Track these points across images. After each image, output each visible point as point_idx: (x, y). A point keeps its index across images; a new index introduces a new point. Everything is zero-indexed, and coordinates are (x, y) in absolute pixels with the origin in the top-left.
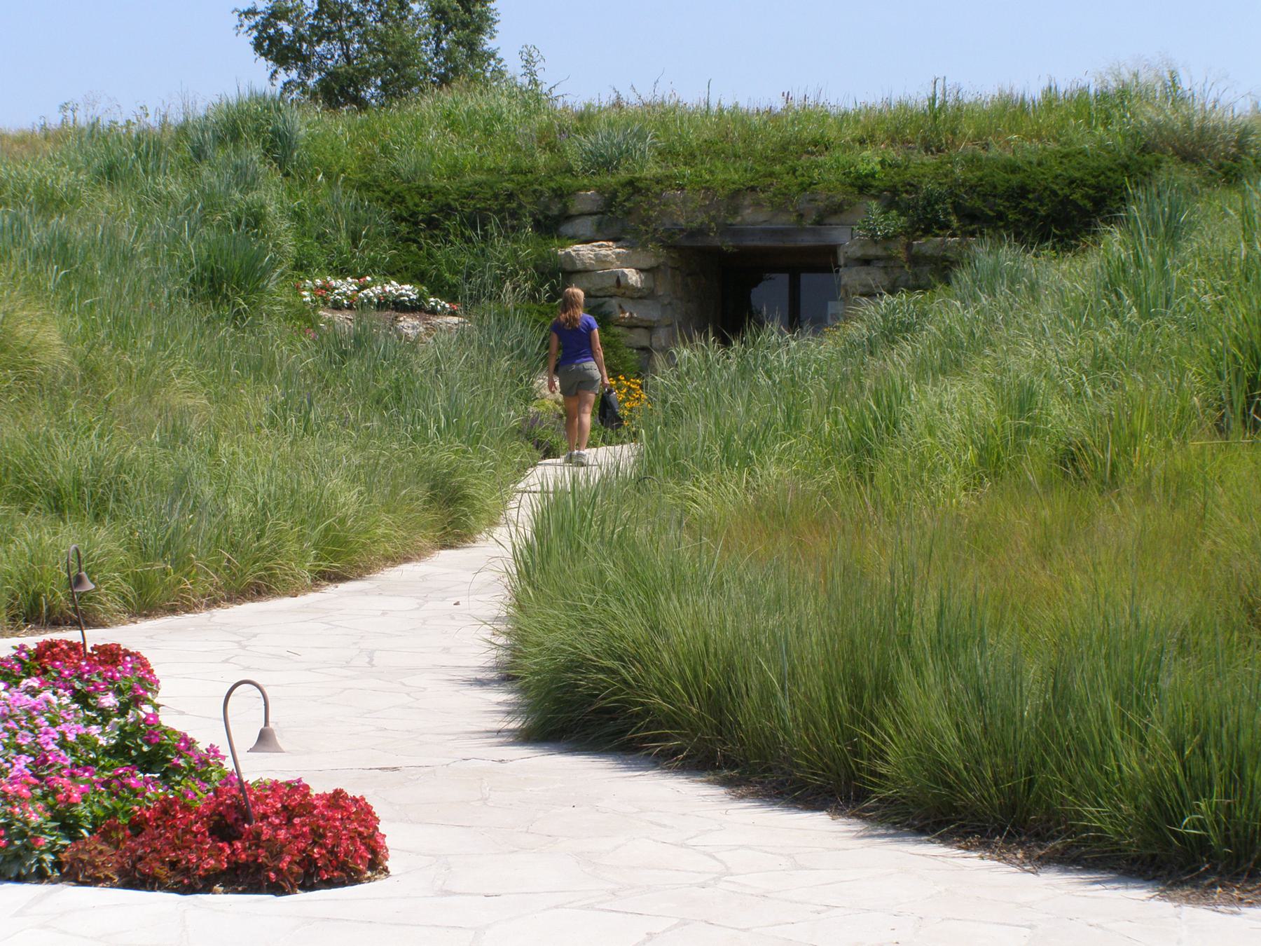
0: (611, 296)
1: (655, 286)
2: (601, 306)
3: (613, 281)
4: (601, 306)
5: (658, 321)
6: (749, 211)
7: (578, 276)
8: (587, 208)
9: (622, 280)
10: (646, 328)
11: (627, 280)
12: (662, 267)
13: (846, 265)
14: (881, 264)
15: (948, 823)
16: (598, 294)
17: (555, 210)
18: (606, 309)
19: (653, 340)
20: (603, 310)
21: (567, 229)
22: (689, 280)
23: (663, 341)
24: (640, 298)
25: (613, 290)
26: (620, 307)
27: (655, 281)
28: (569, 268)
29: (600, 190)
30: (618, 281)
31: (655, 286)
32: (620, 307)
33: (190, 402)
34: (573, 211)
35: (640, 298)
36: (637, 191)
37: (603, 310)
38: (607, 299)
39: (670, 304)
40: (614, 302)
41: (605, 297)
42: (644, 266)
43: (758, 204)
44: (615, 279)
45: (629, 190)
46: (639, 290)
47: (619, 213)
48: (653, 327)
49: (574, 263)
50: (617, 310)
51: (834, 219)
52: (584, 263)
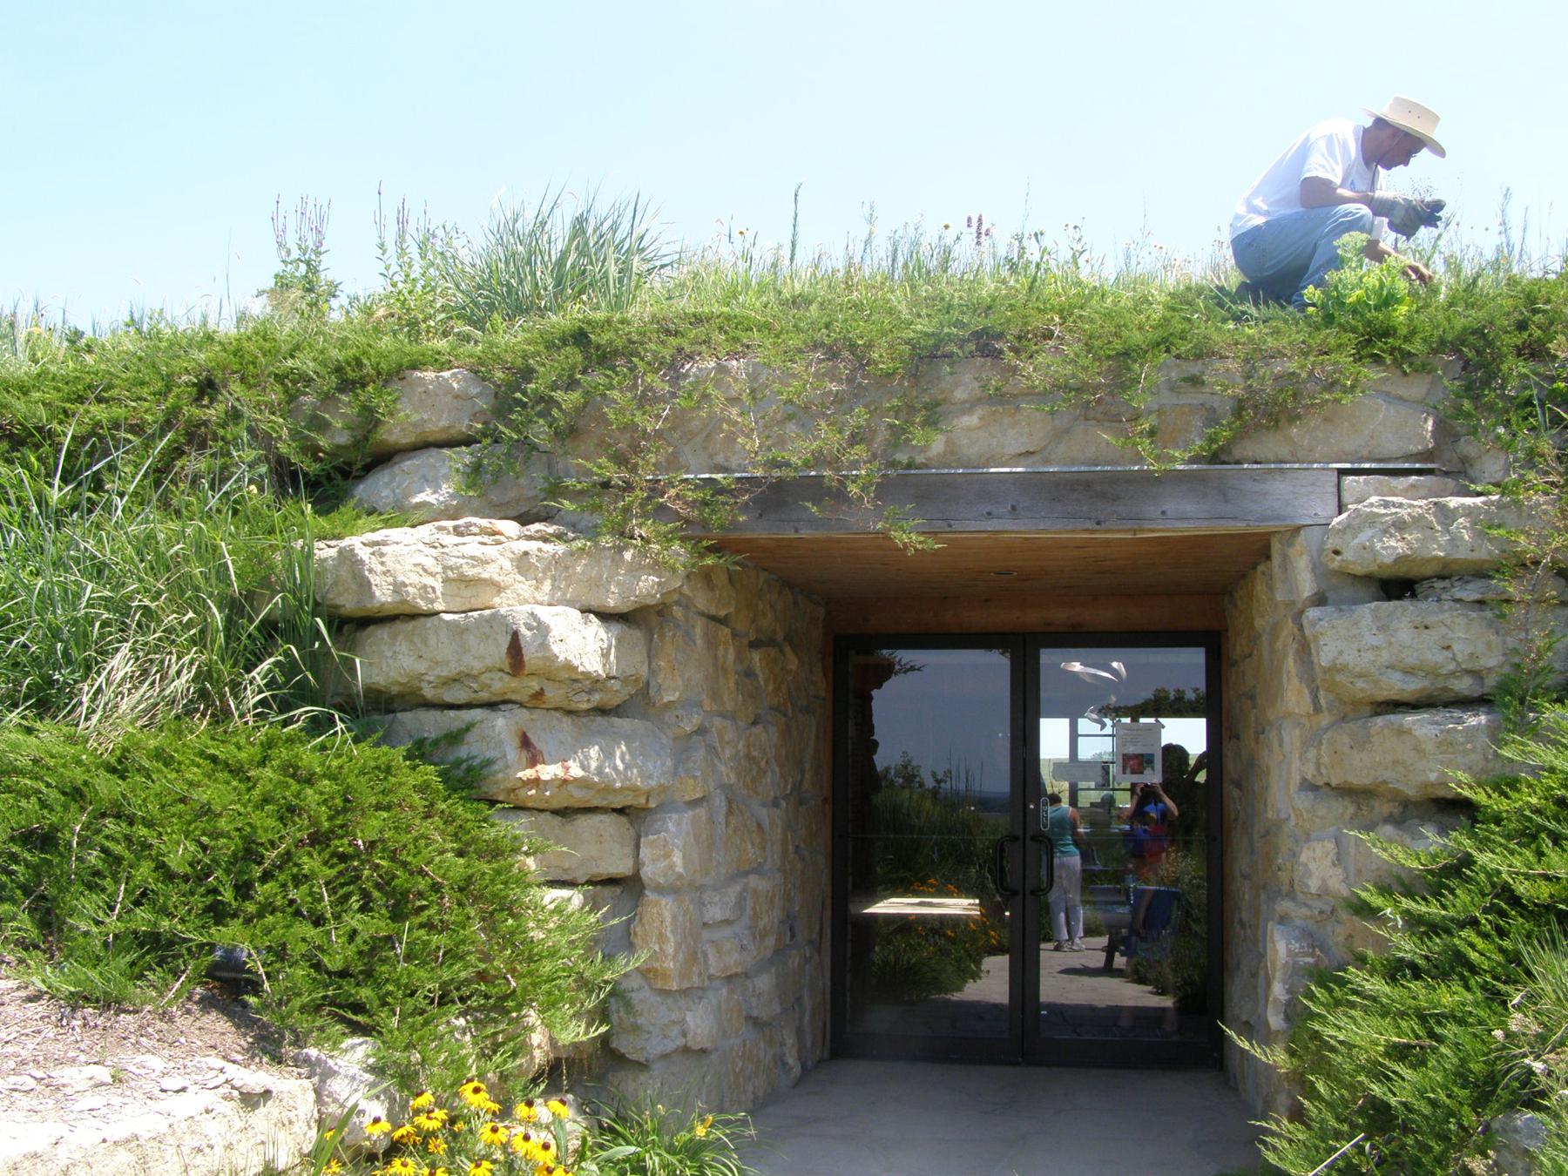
0: (491, 705)
1: (652, 672)
2: (455, 738)
3: (498, 651)
4: (455, 738)
5: (663, 789)
6: (972, 420)
7: (382, 633)
8: (439, 422)
9: (530, 653)
10: (621, 811)
11: (544, 646)
12: (678, 612)
13: (1320, 600)
14: (1471, 592)
15: (547, 518)
16: (449, 697)
17: (337, 434)
18: (472, 748)
19: (645, 853)
20: (463, 752)
21: (378, 486)
22: (756, 657)
23: (677, 857)
24: (602, 711)
25: (501, 684)
26: (525, 743)
27: (651, 656)
28: (348, 603)
29: (478, 371)
30: (515, 647)
31: (652, 672)
32: (525, 743)
33: (726, 698)
34: (393, 432)
35: (602, 711)
36: (604, 358)
37: (463, 752)
38: (477, 714)
39: (701, 731)
40: (502, 724)
41: (469, 706)
42: (612, 600)
43: (1001, 400)
44: (505, 642)
45: (574, 355)
46: (595, 683)
47: (540, 432)
48: (645, 810)
49: (365, 586)
50: (512, 753)
51: (1270, 445)
52: (398, 587)
